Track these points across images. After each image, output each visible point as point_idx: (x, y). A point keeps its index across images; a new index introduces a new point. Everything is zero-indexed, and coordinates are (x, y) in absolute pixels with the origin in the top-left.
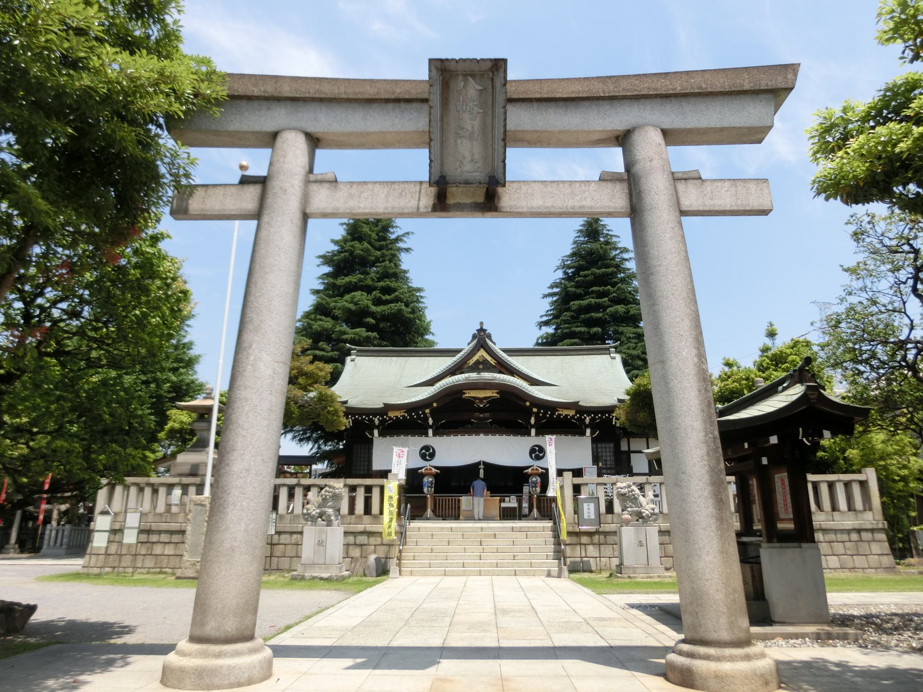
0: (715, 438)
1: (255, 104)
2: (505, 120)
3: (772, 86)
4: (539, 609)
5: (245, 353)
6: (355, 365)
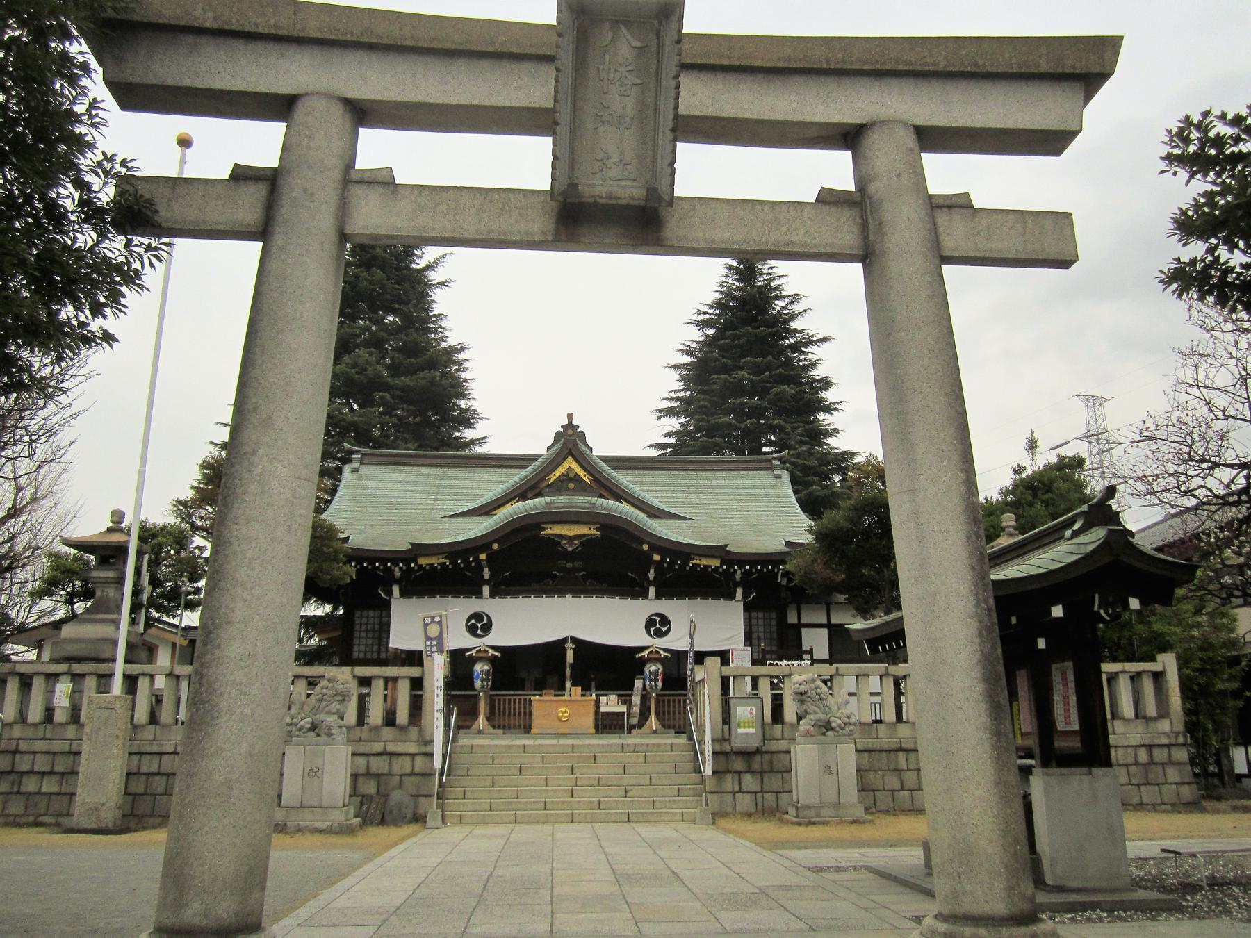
0: (989, 610)
1: (260, 46)
2: (677, 98)
3: (1081, 66)
4: (685, 874)
5: (246, 464)
6: (359, 479)
